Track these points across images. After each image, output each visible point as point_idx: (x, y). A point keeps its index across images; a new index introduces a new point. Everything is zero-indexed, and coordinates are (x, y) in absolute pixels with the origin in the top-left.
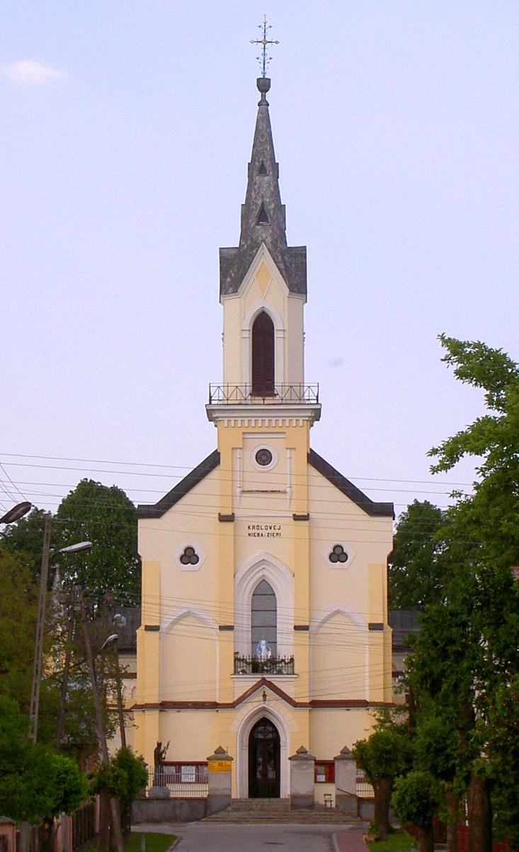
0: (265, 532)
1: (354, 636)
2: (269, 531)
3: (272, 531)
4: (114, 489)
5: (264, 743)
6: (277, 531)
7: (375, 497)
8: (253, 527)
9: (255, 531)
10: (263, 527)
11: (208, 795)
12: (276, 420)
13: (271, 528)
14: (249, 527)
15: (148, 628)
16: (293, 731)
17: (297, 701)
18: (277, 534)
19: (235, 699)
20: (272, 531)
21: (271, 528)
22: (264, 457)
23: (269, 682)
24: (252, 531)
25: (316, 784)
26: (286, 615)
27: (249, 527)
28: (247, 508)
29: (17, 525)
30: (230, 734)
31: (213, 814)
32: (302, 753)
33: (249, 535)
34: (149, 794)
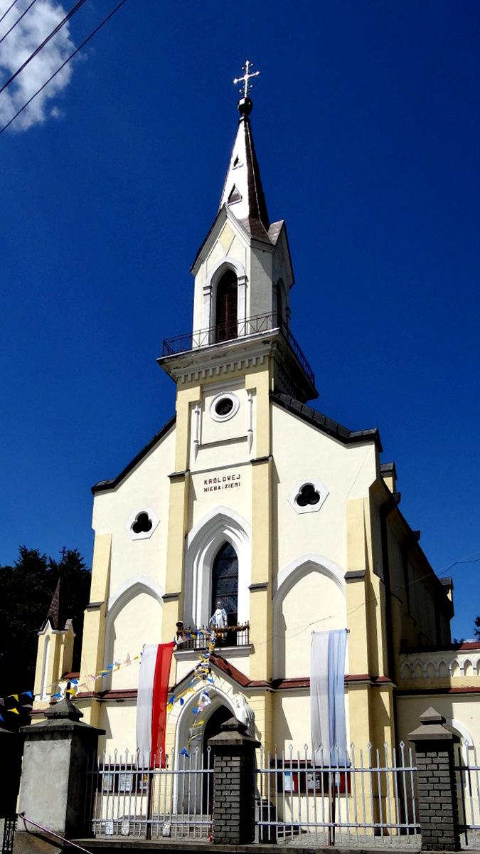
0: (222, 484)
2: (227, 482)
3: (231, 481)
4: (93, 532)
8: (210, 481)
9: (213, 485)
10: (221, 480)
13: (229, 479)
14: (205, 482)
17: (111, 482)
20: (231, 481)
21: (229, 479)
22: (224, 407)
23: (219, 657)
24: (209, 486)
25: (244, 275)
26: (249, 569)
27: (205, 482)
33: (206, 490)
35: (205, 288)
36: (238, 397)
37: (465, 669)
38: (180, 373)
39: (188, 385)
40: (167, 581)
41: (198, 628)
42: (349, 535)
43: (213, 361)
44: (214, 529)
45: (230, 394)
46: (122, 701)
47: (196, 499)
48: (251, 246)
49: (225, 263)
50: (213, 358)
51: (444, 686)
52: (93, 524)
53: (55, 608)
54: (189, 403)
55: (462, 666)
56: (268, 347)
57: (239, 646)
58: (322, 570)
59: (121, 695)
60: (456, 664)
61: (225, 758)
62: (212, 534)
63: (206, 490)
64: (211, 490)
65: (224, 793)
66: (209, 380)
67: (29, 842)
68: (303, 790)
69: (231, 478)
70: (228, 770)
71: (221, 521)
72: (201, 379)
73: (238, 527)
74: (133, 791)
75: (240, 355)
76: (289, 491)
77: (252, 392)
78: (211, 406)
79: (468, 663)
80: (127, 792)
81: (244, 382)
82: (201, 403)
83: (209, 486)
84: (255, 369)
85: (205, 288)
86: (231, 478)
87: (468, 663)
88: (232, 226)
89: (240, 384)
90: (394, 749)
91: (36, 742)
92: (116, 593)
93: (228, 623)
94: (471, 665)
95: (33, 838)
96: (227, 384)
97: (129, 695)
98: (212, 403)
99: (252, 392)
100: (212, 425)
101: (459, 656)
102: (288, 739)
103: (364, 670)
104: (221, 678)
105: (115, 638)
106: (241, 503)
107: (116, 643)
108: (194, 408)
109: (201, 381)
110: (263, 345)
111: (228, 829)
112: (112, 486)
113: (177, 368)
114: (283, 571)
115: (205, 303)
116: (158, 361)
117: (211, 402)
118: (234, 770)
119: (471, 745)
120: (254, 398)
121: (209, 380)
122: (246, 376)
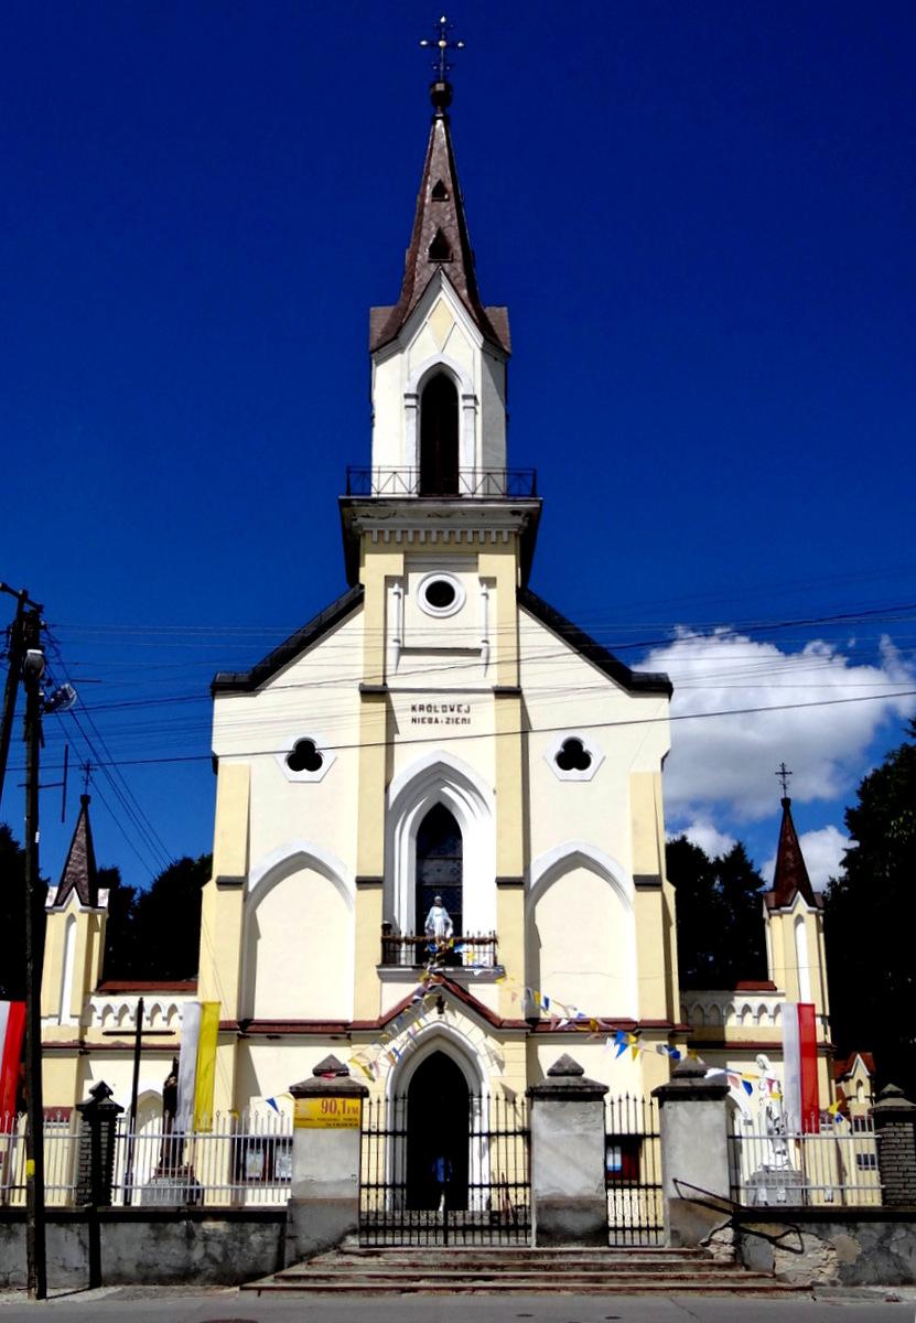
1: (414, 1265)
2: (449, 714)
3: (455, 714)
5: (437, 1099)
6: (461, 716)
7: (485, 934)
8: (422, 708)
11: (290, 1201)
12: (462, 533)
13: (452, 710)
15: (226, 883)
16: (500, 1072)
18: (464, 720)
19: (384, 1012)
20: (455, 714)
22: (440, 595)
24: (419, 714)
26: (484, 853)
28: (406, 674)
29: (441, 1162)
30: (377, 1069)
31: (300, 1258)
32: (566, 1073)
33: (414, 720)
34: (144, 1197)
35: (407, 396)
36: (465, 584)
37: (742, 1016)
38: (371, 525)
39: (384, 547)
40: (358, 859)
41: (436, 935)
42: (635, 824)
43: (429, 521)
44: (428, 782)
45: (452, 577)
46: (277, 1038)
47: (398, 732)
48: (482, 350)
49: (441, 363)
50: (429, 516)
51: (715, 1038)
52: (215, 739)
53: (81, 868)
54: (386, 577)
55: (739, 1012)
56: (518, 520)
57: (401, 966)
58: (592, 865)
59: (277, 1029)
60: (731, 1009)
61: (897, 1124)
62: (425, 789)
63: (414, 720)
64: (423, 722)
65: (900, 1158)
66: (417, 548)
67: (689, 1209)
68: (270, 1179)
69: (456, 709)
70: (902, 1135)
71: (440, 773)
72: (405, 543)
73: (468, 785)
74: (264, 1179)
75: (473, 521)
76: (546, 747)
77: (489, 582)
78: (465, 602)
79: (747, 1009)
80: (257, 1179)
81: (477, 563)
82: (403, 581)
83: (419, 714)
84: (496, 548)
85: (407, 396)
86: (456, 709)
87: (747, 1009)
88: (449, 305)
89: (474, 567)
90: (701, 1196)
91: (680, 1103)
92: (261, 866)
93: (47, 890)
94: (766, 1012)
95: (693, 1204)
96: (450, 560)
97: (289, 1029)
98: (465, 602)
99: (489, 582)
100: (415, 616)
101: (736, 998)
102: (254, 1095)
103: (662, 1016)
104: (457, 1014)
105: (258, 937)
106: (478, 751)
107: (260, 943)
108: (393, 587)
109: (407, 548)
110: (510, 515)
111: (907, 1191)
112: (251, 683)
113: (368, 516)
114: (538, 861)
115: (408, 419)
116: (340, 501)
117: (419, 582)
118: (908, 1135)
119: (749, 1118)
120: (492, 592)
121: (417, 548)
122: (481, 556)
